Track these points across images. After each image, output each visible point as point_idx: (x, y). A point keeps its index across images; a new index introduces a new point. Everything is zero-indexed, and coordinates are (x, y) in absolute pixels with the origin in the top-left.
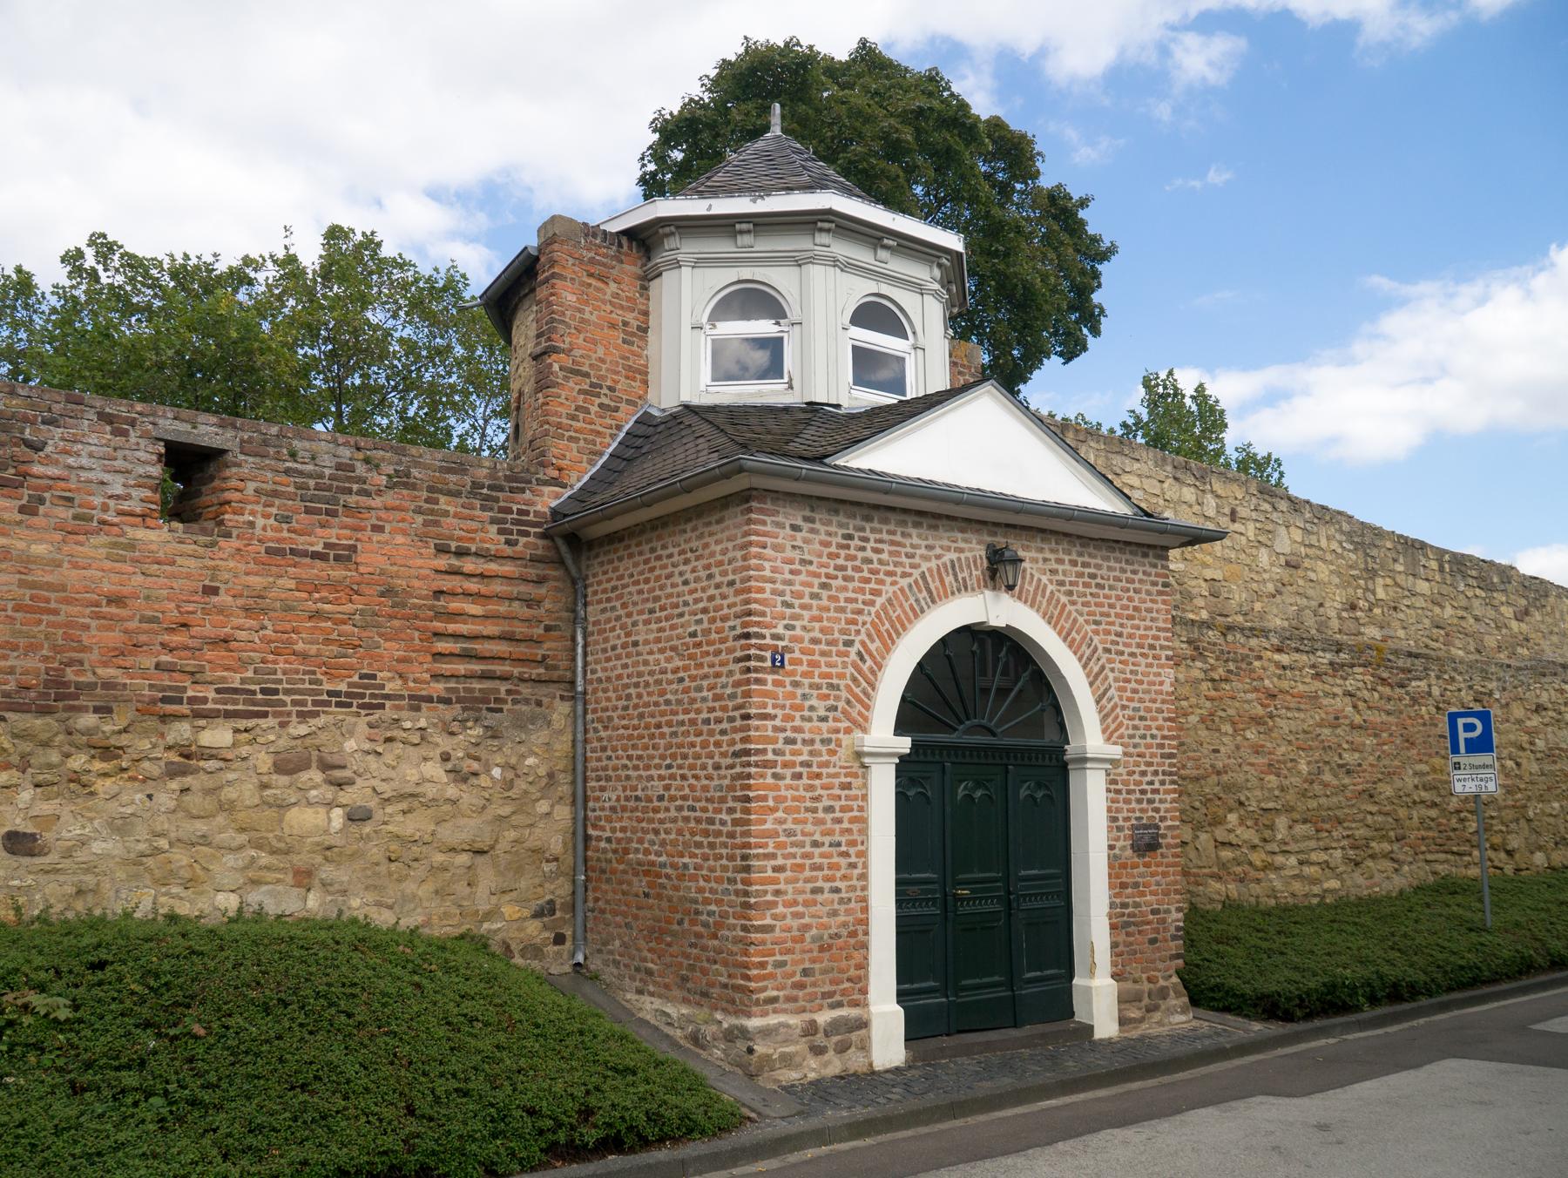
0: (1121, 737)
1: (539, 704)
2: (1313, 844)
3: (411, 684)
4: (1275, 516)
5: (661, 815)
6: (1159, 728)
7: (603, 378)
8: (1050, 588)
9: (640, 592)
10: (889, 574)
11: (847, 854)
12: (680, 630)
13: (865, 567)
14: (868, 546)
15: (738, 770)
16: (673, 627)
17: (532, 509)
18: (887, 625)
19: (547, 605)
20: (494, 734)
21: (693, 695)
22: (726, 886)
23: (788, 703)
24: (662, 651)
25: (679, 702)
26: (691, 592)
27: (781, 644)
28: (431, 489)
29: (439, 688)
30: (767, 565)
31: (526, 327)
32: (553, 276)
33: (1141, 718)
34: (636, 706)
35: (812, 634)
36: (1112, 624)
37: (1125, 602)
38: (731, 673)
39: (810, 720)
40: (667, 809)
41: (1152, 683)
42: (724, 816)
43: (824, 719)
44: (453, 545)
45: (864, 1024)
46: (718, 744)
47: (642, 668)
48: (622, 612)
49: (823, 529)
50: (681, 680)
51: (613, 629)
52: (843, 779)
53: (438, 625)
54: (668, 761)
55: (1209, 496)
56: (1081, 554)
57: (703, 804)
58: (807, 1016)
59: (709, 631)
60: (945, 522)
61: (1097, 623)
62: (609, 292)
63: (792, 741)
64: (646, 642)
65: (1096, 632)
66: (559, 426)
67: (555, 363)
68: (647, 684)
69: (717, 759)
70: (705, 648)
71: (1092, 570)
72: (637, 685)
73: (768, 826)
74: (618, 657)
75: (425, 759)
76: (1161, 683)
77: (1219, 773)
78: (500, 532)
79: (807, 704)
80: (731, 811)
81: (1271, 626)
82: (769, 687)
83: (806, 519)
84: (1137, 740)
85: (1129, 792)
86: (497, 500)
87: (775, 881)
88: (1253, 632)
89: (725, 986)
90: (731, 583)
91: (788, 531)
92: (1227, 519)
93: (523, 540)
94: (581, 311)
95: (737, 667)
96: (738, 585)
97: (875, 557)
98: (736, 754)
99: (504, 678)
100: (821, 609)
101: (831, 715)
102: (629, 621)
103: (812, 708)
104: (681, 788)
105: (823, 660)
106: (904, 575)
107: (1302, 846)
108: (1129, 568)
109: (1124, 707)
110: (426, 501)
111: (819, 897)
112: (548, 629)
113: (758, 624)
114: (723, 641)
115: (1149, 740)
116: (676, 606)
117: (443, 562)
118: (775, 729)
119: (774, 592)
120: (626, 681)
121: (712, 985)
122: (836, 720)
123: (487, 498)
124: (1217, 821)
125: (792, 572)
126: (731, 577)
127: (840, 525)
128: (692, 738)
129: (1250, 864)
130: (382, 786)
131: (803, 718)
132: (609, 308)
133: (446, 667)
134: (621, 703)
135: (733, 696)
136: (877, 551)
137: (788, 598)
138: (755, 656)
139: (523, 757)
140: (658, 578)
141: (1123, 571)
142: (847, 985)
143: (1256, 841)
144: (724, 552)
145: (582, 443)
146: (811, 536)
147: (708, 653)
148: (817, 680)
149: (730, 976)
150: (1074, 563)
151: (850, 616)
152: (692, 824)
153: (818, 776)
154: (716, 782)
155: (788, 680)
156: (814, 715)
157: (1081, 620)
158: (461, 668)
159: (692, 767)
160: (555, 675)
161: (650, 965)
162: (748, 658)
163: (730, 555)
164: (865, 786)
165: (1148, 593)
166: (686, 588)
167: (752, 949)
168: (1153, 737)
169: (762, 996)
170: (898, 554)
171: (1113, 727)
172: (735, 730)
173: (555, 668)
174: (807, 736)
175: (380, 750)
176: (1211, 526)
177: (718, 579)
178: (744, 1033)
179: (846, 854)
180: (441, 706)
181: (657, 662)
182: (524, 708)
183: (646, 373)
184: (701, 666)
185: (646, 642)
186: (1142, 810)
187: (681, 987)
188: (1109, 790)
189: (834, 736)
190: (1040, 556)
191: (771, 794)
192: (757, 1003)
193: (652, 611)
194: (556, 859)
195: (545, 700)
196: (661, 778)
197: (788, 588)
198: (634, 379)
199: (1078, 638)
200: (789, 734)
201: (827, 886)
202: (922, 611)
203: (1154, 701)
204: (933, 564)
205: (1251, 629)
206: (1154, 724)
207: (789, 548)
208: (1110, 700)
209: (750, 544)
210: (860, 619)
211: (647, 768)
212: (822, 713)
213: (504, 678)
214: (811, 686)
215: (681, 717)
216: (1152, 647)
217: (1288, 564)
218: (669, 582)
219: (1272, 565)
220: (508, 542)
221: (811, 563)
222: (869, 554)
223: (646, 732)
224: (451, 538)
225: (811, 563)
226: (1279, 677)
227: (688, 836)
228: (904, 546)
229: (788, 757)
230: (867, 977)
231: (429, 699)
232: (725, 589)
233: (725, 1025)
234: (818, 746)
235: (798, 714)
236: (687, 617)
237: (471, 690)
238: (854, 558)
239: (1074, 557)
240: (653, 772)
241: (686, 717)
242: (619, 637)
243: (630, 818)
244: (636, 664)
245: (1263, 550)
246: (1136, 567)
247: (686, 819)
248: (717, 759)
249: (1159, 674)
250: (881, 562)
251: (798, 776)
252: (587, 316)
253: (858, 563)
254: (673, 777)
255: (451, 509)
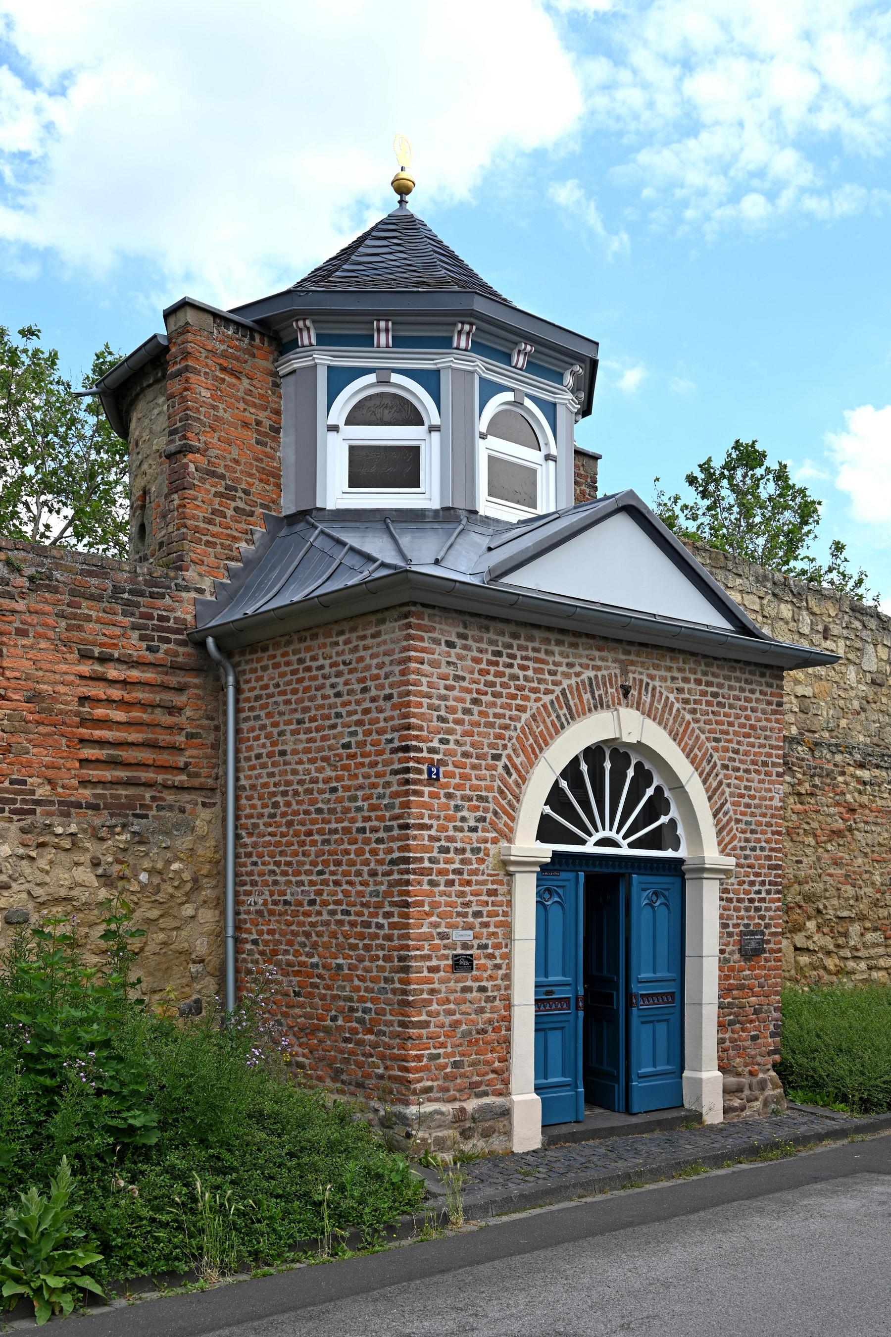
0: (734, 849)
1: (183, 811)
2: (881, 950)
3: (60, 790)
4: (865, 634)
5: (313, 919)
6: (767, 841)
7: (238, 480)
8: (677, 706)
9: (287, 702)
10: (534, 690)
11: (492, 957)
12: (332, 742)
13: (512, 683)
14: (515, 662)
15: (396, 876)
16: (324, 738)
17: (172, 615)
18: (531, 741)
19: (188, 712)
20: (140, 839)
21: (347, 804)
22: (382, 985)
23: (442, 814)
24: (312, 761)
25: (331, 811)
26: (344, 704)
27: (436, 757)
28: (72, 593)
29: (86, 794)
30: (424, 680)
31: (151, 418)
32: (187, 369)
33: (753, 832)
34: (284, 815)
35: (464, 748)
36: (730, 741)
37: (743, 720)
38: (387, 785)
39: (461, 830)
40: (319, 913)
41: (763, 798)
42: (381, 920)
43: (474, 830)
44: (97, 651)
45: (506, 1113)
46: (374, 852)
47: (290, 777)
48: (267, 722)
49: (474, 645)
50: (334, 790)
51: (257, 738)
52: (490, 886)
53: (84, 732)
54: (320, 868)
55: (805, 613)
56: (705, 674)
57: (358, 908)
58: (457, 1105)
59: (364, 743)
60: (584, 640)
61: (717, 740)
62: (242, 388)
63: (446, 850)
64: (295, 752)
65: (716, 749)
66: (197, 530)
67: (192, 463)
68: (296, 793)
69: (372, 865)
70: (359, 760)
71: (715, 689)
72: (285, 794)
73: (425, 929)
74: (264, 766)
75: (77, 864)
76: (771, 799)
77: (800, 884)
78: (142, 638)
79: (459, 814)
80: (388, 915)
81: (852, 742)
82: (426, 798)
83: (461, 636)
84: (748, 852)
85: (739, 900)
86: (137, 605)
87: (430, 981)
88: (836, 749)
89: (381, 1077)
90: (389, 697)
91: (444, 647)
92: (820, 636)
93: (164, 647)
94: (215, 408)
95: (394, 779)
96: (395, 700)
97: (521, 674)
98: (392, 862)
99: (148, 785)
100: (472, 724)
101: (480, 825)
102: (275, 731)
103: (463, 819)
104: (335, 893)
105: (473, 773)
106: (547, 692)
107: (872, 952)
108: (748, 687)
109: (738, 821)
110: (68, 605)
111: (469, 996)
112: (190, 736)
113: (416, 738)
114: (380, 753)
115: (758, 852)
116: (327, 717)
117: (86, 668)
118: (432, 838)
119: (430, 707)
120: (273, 789)
121: (368, 1076)
122: (485, 830)
123: (128, 603)
124: (797, 928)
125: (447, 688)
126: (388, 691)
127: (491, 642)
128: (346, 846)
129: (825, 968)
130: (38, 891)
131: (456, 828)
132: (242, 405)
133: (95, 774)
134: (267, 811)
135: (388, 807)
136: (523, 668)
137: (442, 713)
138: (405, 764)
139: (169, 862)
140: (307, 689)
141: (742, 690)
142: (492, 1076)
143: (831, 947)
144: (380, 666)
145: (219, 549)
146: (464, 652)
147: (362, 765)
148: (468, 792)
149: (386, 1068)
150: (698, 682)
151: (497, 731)
152: (347, 928)
153: (469, 883)
154: (372, 888)
155: (442, 792)
156: (465, 825)
157: (703, 737)
158: (108, 775)
159: (345, 874)
160: (196, 782)
161: (301, 1059)
162: (407, 770)
163: (387, 669)
164: (510, 892)
165: (764, 712)
166: (339, 701)
167: (409, 1044)
168: (762, 849)
169: (418, 1086)
170: (541, 671)
171: (727, 839)
172: (392, 839)
173: (197, 775)
174: (459, 845)
175: (33, 854)
176: (805, 645)
177: (374, 692)
178: (404, 1120)
179: (492, 957)
180: (90, 812)
181: (308, 772)
182: (168, 814)
183: (279, 477)
184: (356, 776)
185: (295, 752)
186: (749, 918)
187: (335, 1079)
188: (721, 899)
189: (482, 846)
190: (669, 674)
191: (427, 900)
192: (414, 1093)
193: (300, 722)
194: (202, 961)
195: (189, 807)
196: (312, 883)
197: (443, 703)
198: (267, 483)
199: (700, 754)
200: (443, 843)
201: (476, 985)
202: (563, 727)
203: (764, 815)
204: (573, 681)
205: (836, 745)
206: (763, 837)
207: (444, 664)
208: (726, 814)
209: (409, 659)
210: (507, 734)
211: (297, 873)
212: (472, 823)
213: (148, 785)
214: (463, 798)
215: (334, 826)
216: (765, 764)
217: (873, 682)
218: (319, 694)
219: (859, 682)
220: (149, 649)
221: (464, 679)
222: (516, 670)
223: (295, 839)
224: (94, 644)
225: (464, 679)
226: (860, 793)
227: (341, 939)
228: (547, 663)
229: (442, 866)
230: (508, 1069)
231: (78, 805)
232: (381, 703)
233: (382, 1113)
234: (468, 855)
235: (451, 825)
236: (339, 729)
237: (119, 797)
238: (502, 675)
239: (699, 676)
240: (303, 877)
241: (339, 826)
242: (264, 746)
243: (278, 922)
244: (284, 773)
245: (851, 667)
246: (754, 686)
247: (340, 923)
248: (372, 865)
249: (770, 790)
250: (526, 678)
251: (451, 883)
252: (221, 413)
253: (505, 679)
254: (325, 883)
255: (93, 613)
